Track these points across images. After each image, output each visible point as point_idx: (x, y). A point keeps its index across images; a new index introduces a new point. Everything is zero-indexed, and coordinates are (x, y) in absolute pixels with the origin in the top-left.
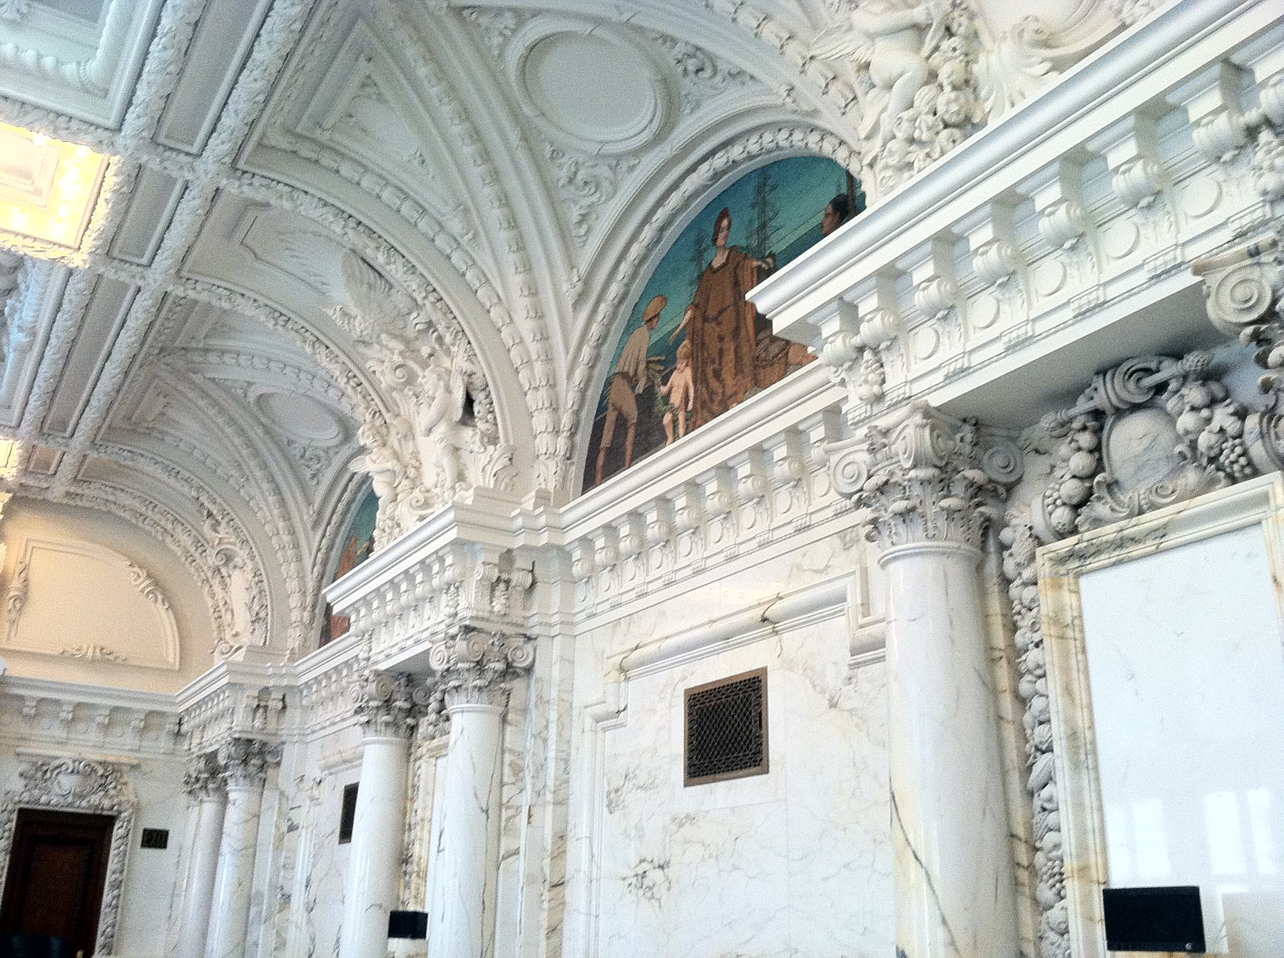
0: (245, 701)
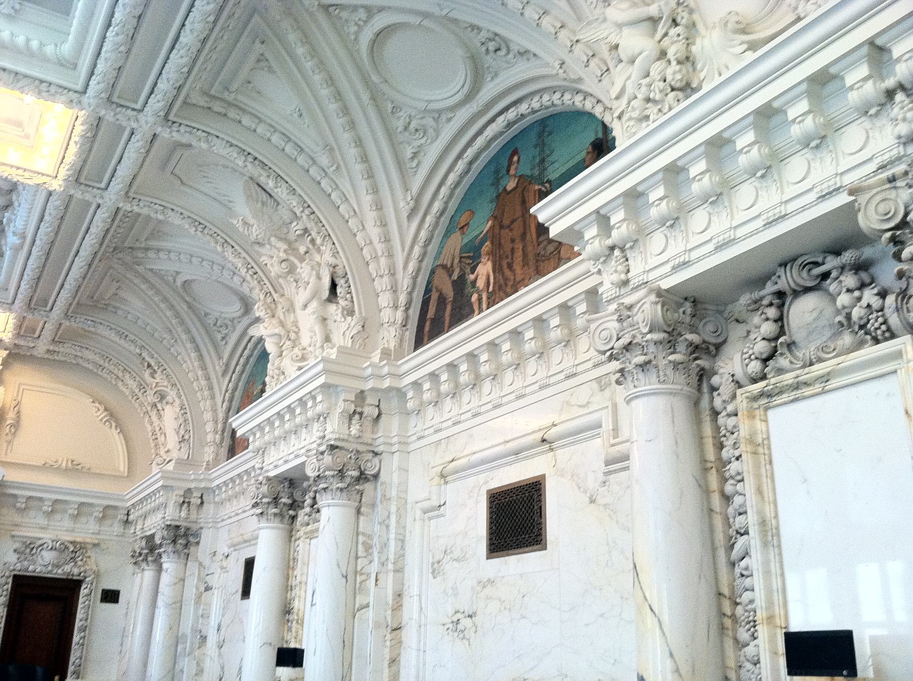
0: (174, 498)
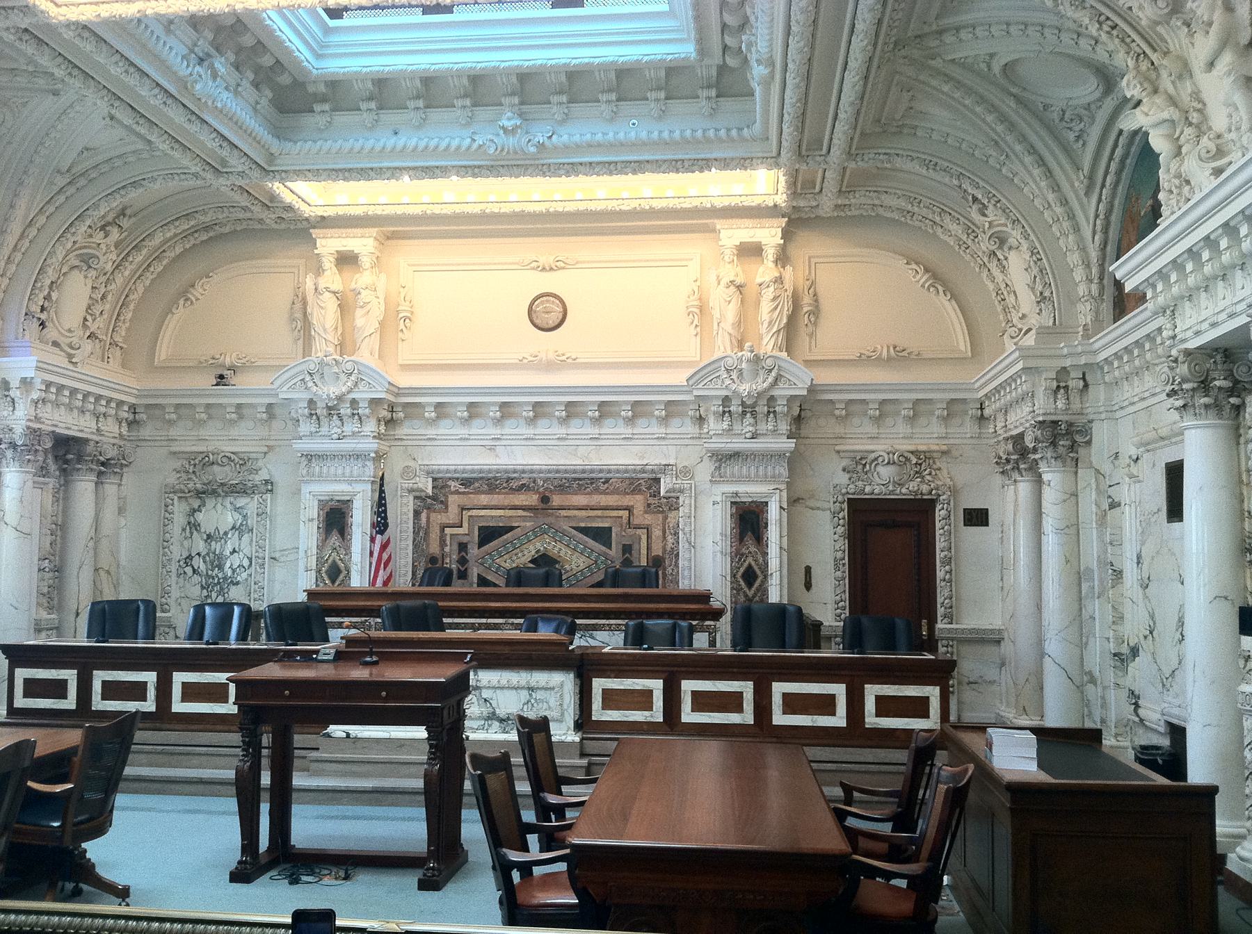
0: (1043, 385)
